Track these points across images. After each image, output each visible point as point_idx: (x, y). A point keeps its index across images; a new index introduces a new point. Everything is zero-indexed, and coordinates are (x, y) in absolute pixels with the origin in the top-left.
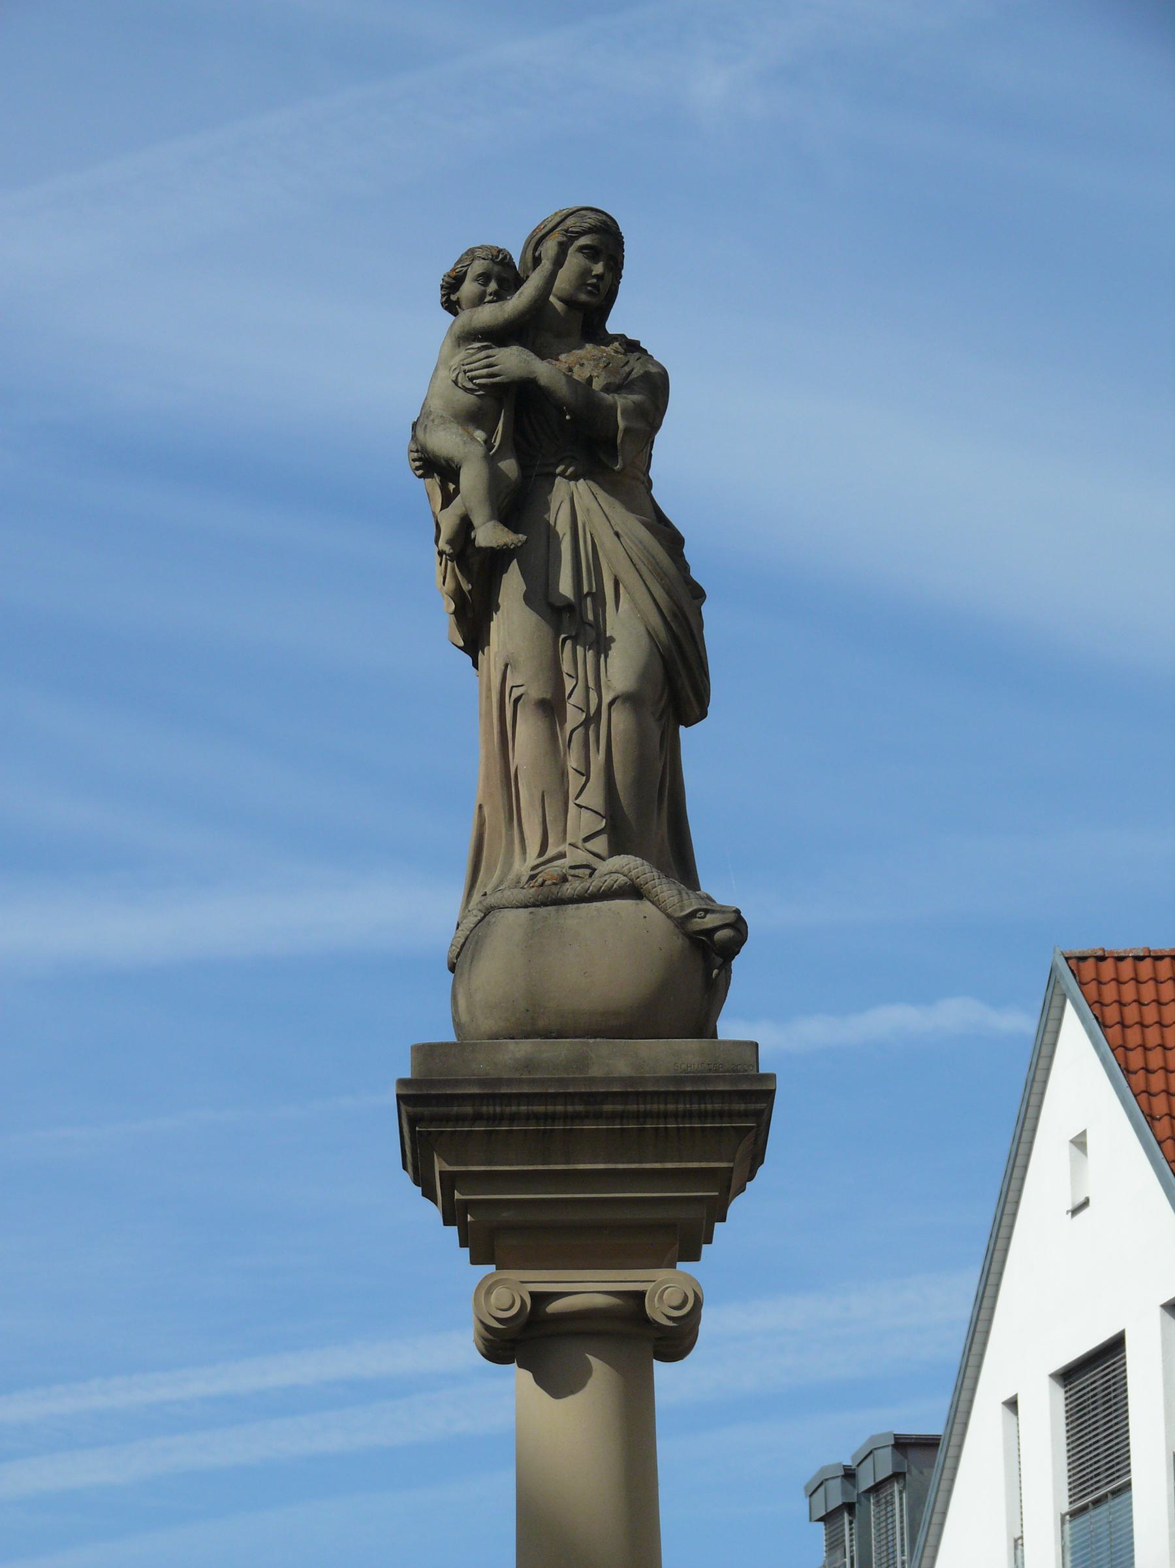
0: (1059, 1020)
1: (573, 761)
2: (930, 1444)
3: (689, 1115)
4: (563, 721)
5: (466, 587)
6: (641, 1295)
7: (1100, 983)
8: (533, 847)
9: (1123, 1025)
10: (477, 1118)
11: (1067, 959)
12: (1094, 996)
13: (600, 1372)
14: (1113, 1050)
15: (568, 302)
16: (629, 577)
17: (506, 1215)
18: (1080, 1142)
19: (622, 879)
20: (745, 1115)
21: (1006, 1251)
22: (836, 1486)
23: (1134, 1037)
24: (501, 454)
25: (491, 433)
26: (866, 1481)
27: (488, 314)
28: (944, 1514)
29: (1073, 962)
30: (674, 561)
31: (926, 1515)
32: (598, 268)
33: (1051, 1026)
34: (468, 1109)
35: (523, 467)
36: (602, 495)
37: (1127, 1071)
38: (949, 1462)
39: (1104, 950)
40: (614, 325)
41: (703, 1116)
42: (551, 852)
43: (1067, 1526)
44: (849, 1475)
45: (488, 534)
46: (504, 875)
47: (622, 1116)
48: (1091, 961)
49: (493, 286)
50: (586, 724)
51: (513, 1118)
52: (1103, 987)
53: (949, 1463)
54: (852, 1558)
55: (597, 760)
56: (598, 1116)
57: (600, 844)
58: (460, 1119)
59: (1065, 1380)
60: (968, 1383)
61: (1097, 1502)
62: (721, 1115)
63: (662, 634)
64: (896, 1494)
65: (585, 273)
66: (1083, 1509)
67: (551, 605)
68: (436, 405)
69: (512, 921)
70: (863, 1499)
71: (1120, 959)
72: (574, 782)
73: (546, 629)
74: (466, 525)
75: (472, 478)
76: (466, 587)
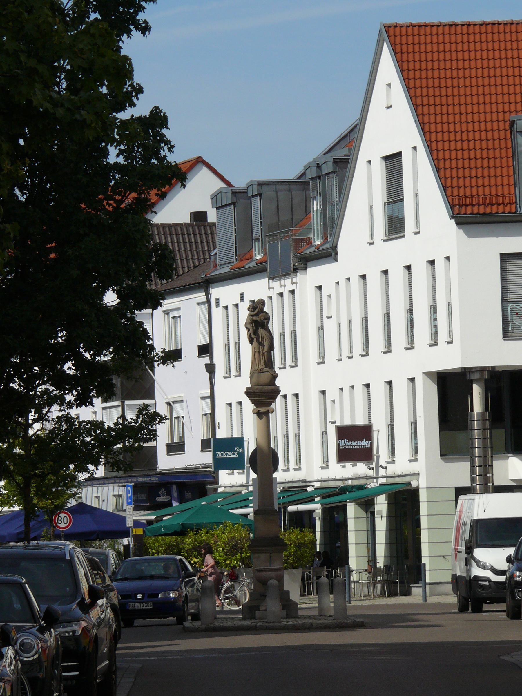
0: (382, 48)
1: (261, 358)
8: (258, 365)
9: (402, 52)
11: (385, 27)
12: (393, 42)
13: (264, 417)
16: (266, 339)
22: (314, 169)
27: (253, 313)
28: (349, 191)
31: (345, 186)
38: (350, 176)
39: (397, 23)
45: (253, 336)
52: (396, 37)
54: (320, 193)
55: (264, 357)
57: (264, 366)
59: (386, 159)
71: (402, 26)
72: (261, 360)
73: (258, 344)
75: (251, 330)
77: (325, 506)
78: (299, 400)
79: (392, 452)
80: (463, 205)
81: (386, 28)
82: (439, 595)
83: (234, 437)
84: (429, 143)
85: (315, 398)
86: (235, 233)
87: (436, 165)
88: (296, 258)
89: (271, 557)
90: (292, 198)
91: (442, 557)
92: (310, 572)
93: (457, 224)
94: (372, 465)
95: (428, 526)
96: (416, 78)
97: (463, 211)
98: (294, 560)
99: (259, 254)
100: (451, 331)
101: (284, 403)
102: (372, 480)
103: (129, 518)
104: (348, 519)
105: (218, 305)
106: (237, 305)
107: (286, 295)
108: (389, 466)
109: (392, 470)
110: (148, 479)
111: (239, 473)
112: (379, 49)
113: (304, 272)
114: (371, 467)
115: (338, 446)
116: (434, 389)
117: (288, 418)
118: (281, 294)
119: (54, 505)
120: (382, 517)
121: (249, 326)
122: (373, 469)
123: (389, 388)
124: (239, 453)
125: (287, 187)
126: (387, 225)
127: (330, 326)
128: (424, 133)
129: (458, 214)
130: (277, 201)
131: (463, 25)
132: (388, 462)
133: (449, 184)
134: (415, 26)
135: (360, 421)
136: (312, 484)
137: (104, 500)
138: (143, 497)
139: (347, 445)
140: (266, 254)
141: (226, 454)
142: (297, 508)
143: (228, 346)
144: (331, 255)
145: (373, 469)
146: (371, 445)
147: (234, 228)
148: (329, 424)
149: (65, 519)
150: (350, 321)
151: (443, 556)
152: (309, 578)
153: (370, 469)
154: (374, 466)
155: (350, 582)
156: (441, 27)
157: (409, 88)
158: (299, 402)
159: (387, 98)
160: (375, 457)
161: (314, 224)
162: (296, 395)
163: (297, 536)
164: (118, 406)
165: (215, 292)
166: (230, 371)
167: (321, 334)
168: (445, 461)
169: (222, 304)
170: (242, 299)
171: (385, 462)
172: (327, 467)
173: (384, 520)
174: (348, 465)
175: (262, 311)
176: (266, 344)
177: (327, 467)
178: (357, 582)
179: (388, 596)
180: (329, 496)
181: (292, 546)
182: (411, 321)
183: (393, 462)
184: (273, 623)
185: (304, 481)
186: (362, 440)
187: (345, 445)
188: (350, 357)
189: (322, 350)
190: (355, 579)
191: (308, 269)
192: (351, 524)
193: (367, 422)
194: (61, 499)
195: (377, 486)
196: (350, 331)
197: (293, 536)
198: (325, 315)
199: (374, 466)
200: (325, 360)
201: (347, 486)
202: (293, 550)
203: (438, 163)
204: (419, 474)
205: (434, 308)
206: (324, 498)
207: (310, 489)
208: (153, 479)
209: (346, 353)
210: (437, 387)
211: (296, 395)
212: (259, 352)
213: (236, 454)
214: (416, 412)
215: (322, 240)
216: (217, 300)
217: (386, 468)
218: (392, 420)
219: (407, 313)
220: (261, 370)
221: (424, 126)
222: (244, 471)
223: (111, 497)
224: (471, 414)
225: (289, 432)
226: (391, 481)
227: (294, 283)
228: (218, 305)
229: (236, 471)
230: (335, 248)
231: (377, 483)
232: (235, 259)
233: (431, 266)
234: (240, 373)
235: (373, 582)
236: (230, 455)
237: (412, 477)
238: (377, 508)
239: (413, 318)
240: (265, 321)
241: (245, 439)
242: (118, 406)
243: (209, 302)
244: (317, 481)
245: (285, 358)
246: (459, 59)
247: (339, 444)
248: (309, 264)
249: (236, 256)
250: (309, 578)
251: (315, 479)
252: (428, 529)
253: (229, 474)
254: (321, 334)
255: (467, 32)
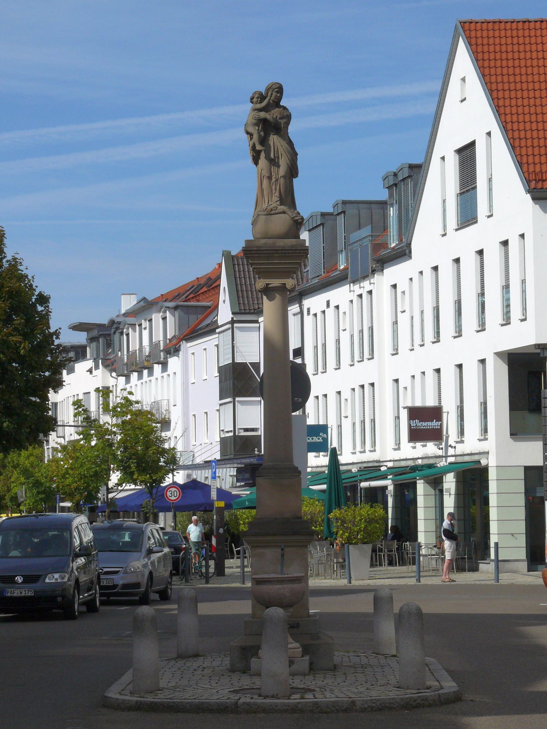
1: (273, 188)
2: (418, 167)
3: (293, 253)
4: (272, 180)
5: (255, 155)
6: (285, 284)
7: (470, 31)
8: (267, 203)
10: (256, 254)
11: (460, 23)
14: (473, 53)
15: (273, 101)
17: (262, 270)
18: (463, 80)
19: (282, 210)
20: (303, 253)
21: (443, 107)
22: (391, 178)
23: (480, 49)
24: (260, 131)
25: (259, 127)
26: (400, 178)
27: (259, 106)
29: (462, 24)
30: (291, 149)
32: (279, 95)
33: (455, 43)
34: (254, 252)
35: (265, 133)
36: (279, 138)
37: (477, 60)
40: (282, 103)
41: (296, 253)
42: (270, 204)
43: (459, 197)
44: (395, 175)
45: (258, 147)
46: (261, 208)
47: (282, 253)
48: (468, 23)
49: (259, 99)
50: (276, 181)
51: (262, 254)
53: (425, 172)
54: (396, 200)
55: (278, 187)
56: (277, 253)
57: (278, 203)
58: (253, 254)
60: (430, 151)
61: (467, 191)
62: (299, 253)
63: (290, 164)
64: (409, 182)
65: (276, 96)
66: (464, 192)
67: (270, 159)
68: (249, 122)
69: (262, 218)
70: (400, 182)
71: (477, 23)
73: (269, 164)
74: (254, 145)
75: (255, 137)
76: (255, 155)
77: (396, 483)
78: (375, 389)
79: (462, 432)
80: (539, 180)
81: (462, 23)
82: (507, 572)
83: (320, 424)
84: (504, 124)
85: (389, 386)
86: (323, 250)
87: (512, 143)
88: (374, 260)
89: (283, 555)
90: (372, 216)
91: (511, 535)
92: (382, 545)
93: (534, 199)
94: (441, 445)
95: (498, 503)
96: (491, 66)
97: (539, 185)
98: (364, 535)
99: (342, 265)
100: (524, 309)
101: (362, 392)
102: (441, 459)
103: (213, 491)
104: (418, 496)
105: (309, 313)
106: (324, 312)
107: (365, 296)
108: (458, 446)
109: (461, 449)
110: (249, 461)
111: (324, 456)
112: (454, 47)
113: (380, 273)
114: (441, 447)
115: (410, 426)
116: (504, 369)
117: (365, 408)
118: (360, 296)
119: (152, 479)
120: (450, 494)
121: (251, 129)
122: (442, 449)
123: (459, 372)
124: (323, 438)
125: (368, 205)
126: (459, 215)
127: (404, 320)
128: (499, 115)
129: (534, 189)
130: (359, 218)
131: (536, 21)
132: (457, 442)
133: (524, 160)
134: (489, 22)
135: (431, 402)
136: (385, 464)
137: (223, 479)
138: (247, 476)
139: (418, 425)
140: (348, 264)
141: (312, 439)
142: (369, 484)
143: (316, 347)
144: (405, 254)
145: (442, 449)
146: (441, 425)
147: (322, 245)
148: (401, 409)
149: (175, 492)
150: (422, 312)
151: (512, 534)
152: (381, 550)
153: (439, 449)
154: (443, 445)
155: (419, 555)
156: (515, 23)
157: (484, 76)
158: (375, 390)
159: (461, 93)
160: (445, 437)
161: (390, 240)
162: (372, 385)
163: (368, 511)
164: (230, 402)
165: (308, 303)
166: (318, 370)
167: (395, 329)
168: (515, 440)
169: (312, 312)
170: (328, 305)
171: (455, 442)
172: (399, 449)
173: (453, 497)
174: (419, 445)
175: (277, 103)
176: (283, 163)
177: (399, 449)
178: (426, 556)
179: (456, 572)
180: (401, 475)
181: (363, 521)
182: (482, 305)
183: (462, 442)
184: (273, 697)
185: (379, 461)
186: (432, 421)
187: (416, 426)
188: (422, 345)
189: (396, 343)
190: (424, 553)
191: (385, 271)
192: (421, 501)
193: (437, 404)
194: (159, 474)
195: (446, 464)
196: (422, 321)
197: (364, 511)
198: (399, 309)
199: (443, 445)
200: (399, 351)
201: (417, 465)
202: (363, 526)
203: (514, 142)
204: (488, 453)
205: (506, 287)
206: (396, 476)
207: (383, 469)
208: (252, 460)
209: (417, 341)
210: (506, 367)
211: (372, 385)
212: (270, 178)
213: (320, 439)
214: (486, 392)
215: (397, 242)
216: (309, 310)
217: (455, 447)
218: (462, 401)
219: (479, 297)
220: (272, 210)
221: (499, 109)
222: (328, 454)
223: (228, 476)
224: (544, 392)
225: (365, 418)
226: (460, 459)
227: (372, 283)
228: (309, 313)
229: (321, 454)
230: (409, 245)
231: (446, 462)
232: (323, 272)
233: (503, 247)
234: (326, 370)
235: (442, 558)
236: (316, 439)
237: (482, 456)
238: (446, 486)
239: (484, 301)
240: (282, 121)
241: (329, 426)
242: (230, 402)
243: (301, 312)
244: (390, 461)
245: (363, 352)
246: (533, 51)
247: (410, 424)
248: (385, 265)
249: (324, 269)
250: (381, 550)
251: (389, 459)
252: (497, 507)
253: (316, 457)
254: (395, 329)
255: (539, 27)
